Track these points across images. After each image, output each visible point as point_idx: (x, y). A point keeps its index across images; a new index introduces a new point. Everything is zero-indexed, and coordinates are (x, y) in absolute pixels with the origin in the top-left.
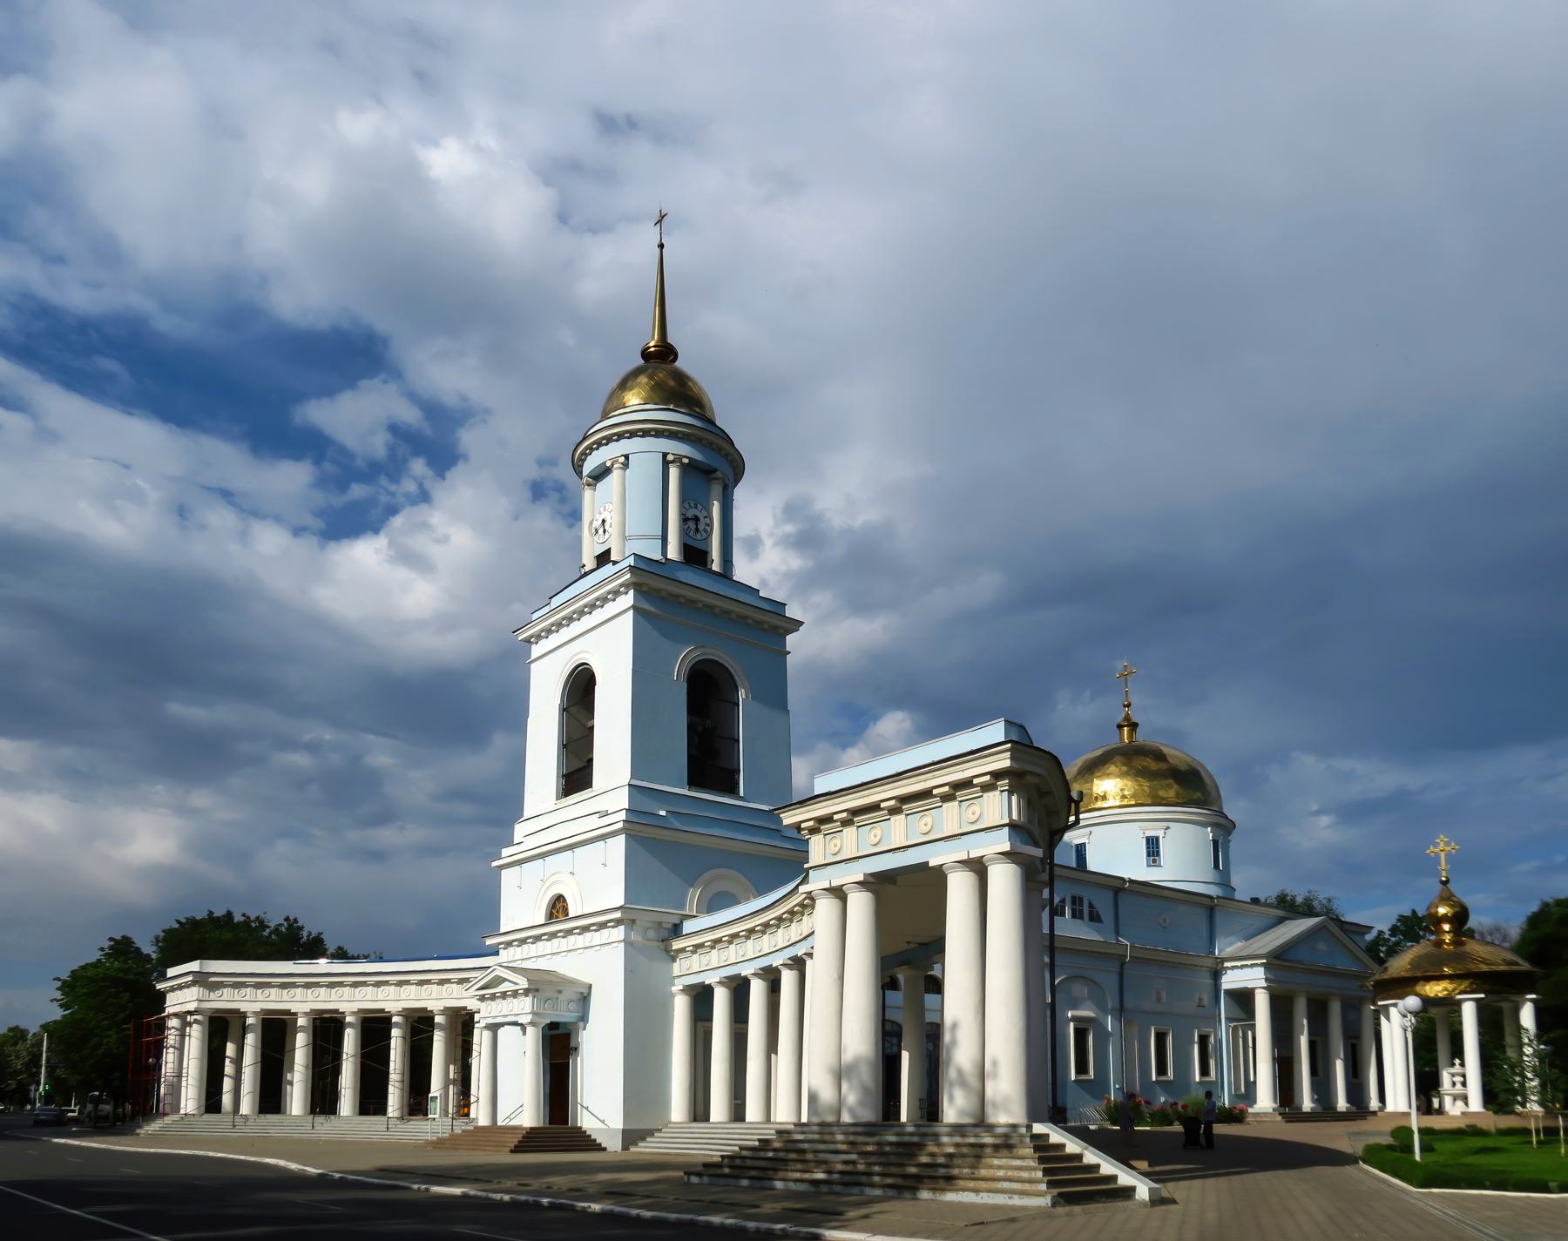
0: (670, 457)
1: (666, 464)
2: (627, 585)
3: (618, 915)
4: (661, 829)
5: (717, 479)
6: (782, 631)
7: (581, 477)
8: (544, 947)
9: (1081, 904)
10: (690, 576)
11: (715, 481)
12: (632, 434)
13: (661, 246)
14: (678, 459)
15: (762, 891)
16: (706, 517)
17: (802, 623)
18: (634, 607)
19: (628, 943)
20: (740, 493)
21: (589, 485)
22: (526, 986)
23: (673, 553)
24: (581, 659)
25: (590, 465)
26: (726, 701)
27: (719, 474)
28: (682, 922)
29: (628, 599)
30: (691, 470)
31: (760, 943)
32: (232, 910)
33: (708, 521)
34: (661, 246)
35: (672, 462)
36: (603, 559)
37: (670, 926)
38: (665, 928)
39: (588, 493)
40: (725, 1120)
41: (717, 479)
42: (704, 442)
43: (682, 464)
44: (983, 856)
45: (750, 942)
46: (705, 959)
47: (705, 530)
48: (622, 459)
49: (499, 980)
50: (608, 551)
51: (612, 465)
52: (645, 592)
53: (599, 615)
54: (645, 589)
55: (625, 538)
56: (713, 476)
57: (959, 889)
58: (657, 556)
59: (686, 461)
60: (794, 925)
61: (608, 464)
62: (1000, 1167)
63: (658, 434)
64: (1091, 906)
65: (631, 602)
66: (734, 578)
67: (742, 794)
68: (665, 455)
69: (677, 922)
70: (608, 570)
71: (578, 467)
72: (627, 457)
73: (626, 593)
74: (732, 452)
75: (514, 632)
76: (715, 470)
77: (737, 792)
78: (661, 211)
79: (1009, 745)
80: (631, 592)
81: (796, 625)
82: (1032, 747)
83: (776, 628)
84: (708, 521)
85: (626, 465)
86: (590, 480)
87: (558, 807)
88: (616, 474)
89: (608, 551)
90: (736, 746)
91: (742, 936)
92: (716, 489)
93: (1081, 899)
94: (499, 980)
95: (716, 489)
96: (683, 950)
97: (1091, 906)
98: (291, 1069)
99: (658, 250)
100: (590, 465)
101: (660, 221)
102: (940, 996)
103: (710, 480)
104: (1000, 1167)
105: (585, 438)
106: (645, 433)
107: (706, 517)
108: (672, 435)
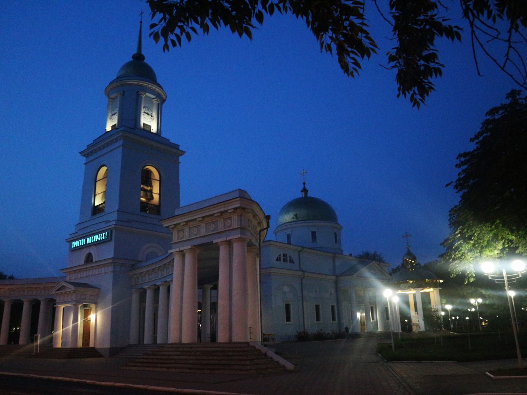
3: (110, 261)
8: (84, 274)
9: (287, 257)
13: (141, 22)
17: (185, 152)
19: (114, 272)
22: (74, 290)
29: (121, 142)
32: (271, 217)
34: (141, 22)
40: (151, 343)
44: (232, 239)
49: (63, 287)
53: (111, 148)
57: (223, 253)
62: (216, 360)
64: (290, 257)
66: (162, 136)
79: (239, 199)
81: (183, 153)
82: (252, 200)
87: (91, 219)
90: (101, 206)
93: (286, 255)
94: (63, 287)
97: (290, 257)
98: (406, 294)
99: (140, 24)
102: (216, 291)
104: (216, 360)
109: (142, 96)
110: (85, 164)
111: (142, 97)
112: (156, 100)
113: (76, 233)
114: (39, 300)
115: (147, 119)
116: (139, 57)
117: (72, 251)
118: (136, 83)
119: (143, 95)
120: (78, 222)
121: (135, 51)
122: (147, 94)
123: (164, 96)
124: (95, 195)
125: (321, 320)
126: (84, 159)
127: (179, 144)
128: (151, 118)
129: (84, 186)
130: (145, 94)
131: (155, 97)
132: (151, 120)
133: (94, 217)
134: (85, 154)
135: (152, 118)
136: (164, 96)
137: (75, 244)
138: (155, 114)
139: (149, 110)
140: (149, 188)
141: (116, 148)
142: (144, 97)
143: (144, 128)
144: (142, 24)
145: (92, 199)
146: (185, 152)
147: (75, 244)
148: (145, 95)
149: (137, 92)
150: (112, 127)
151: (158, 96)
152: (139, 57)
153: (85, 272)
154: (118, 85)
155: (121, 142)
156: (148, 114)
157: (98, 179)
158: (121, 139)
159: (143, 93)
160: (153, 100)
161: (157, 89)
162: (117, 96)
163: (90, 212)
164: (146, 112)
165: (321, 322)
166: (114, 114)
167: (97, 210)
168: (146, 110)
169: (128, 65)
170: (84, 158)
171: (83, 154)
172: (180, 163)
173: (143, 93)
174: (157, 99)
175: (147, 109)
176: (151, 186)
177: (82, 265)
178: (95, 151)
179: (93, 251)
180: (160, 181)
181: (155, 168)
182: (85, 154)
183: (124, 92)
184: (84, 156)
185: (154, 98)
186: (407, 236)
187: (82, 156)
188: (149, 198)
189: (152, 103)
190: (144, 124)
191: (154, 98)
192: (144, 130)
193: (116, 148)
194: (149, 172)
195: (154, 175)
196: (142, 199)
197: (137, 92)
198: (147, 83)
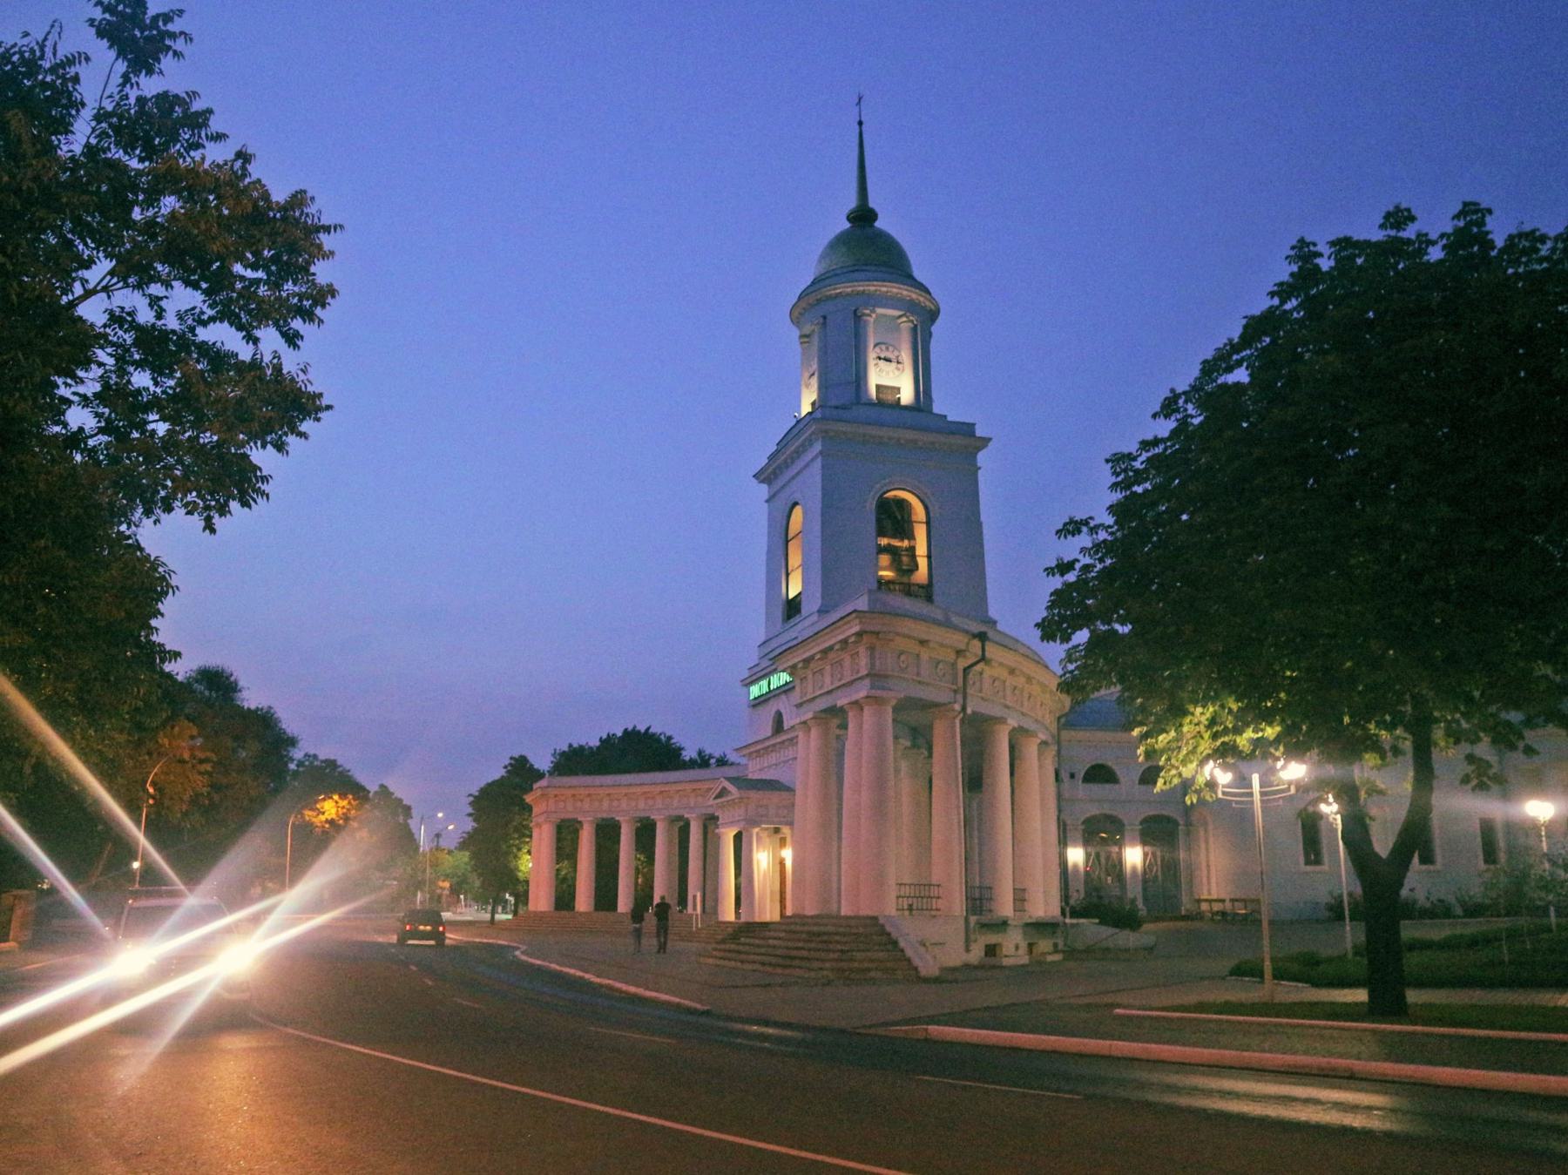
8: (773, 758)
13: (860, 123)
22: (738, 796)
34: (860, 123)
53: (800, 464)
81: (985, 441)
99: (857, 127)
109: (865, 318)
110: (767, 501)
111: (865, 321)
112: (904, 319)
113: (757, 665)
114: (687, 819)
115: (888, 373)
116: (863, 216)
117: (754, 706)
118: (849, 290)
119: (870, 315)
120: (763, 639)
121: (852, 203)
122: (880, 311)
123: (928, 303)
124: (787, 575)
125: (1439, 858)
126: (763, 490)
127: (971, 421)
128: (898, 369)
129: (769, 552)
130: (874, 312)
131: (901, 313)
132: (897, 373)
133: (792, 622)
134: (766, 476)
135: (900, 366)
136: (928, 303)
137: (755, 691)
138: (906, 357)
139: (891, 349)
140: (906, 543)
141: (807, 466)
142: (872, 320)
143: (881, 395)
144: (863, 126)
145: (781, 583)
146: (990, 439)
147: (755, 691)
148: (874, 315)
149: (855, 311)
150: (813, 404)
151: (911, 307)
152: (863, 216)
153: (773, 754)
154: (811, 301)
155: (818, 447)
156: (888, 360)
157: (791, 535)
158: (817, 440)
159: (868, 312)
160: (900, 321)
161: (905, 293)
162: (813, 331)
163: (779, 613)
164: (882, 356)
165: (1438, 866)
166: (813, 374)
167: (793, 608)
168: (882, 350)
169: (841, 240)
170: (764, 487)
171: (762, 477)
172: (980, 468)
173: (868, 312)
174: (907, 317)
175: (883, 347)
176: (911, 537)
177: (768, 738)
178: (787, 465)
179: (783, 705)
180: (928, 523)
181: (913, 494)
182: (766, 476)
183: (825, 318)
184: (762, 482)
185: (900, 317)
186: (185, 1113)
187: (760, 482)
188: (904, 567)
189: (898, 329)
190: (878, 387)
191: (900, 317)
192: (880, 403)
193: (807, 466)
194: (902, 504)
195: (916, 514)
196: (881, 573)
197: (855, 311)
198: (875, 283)
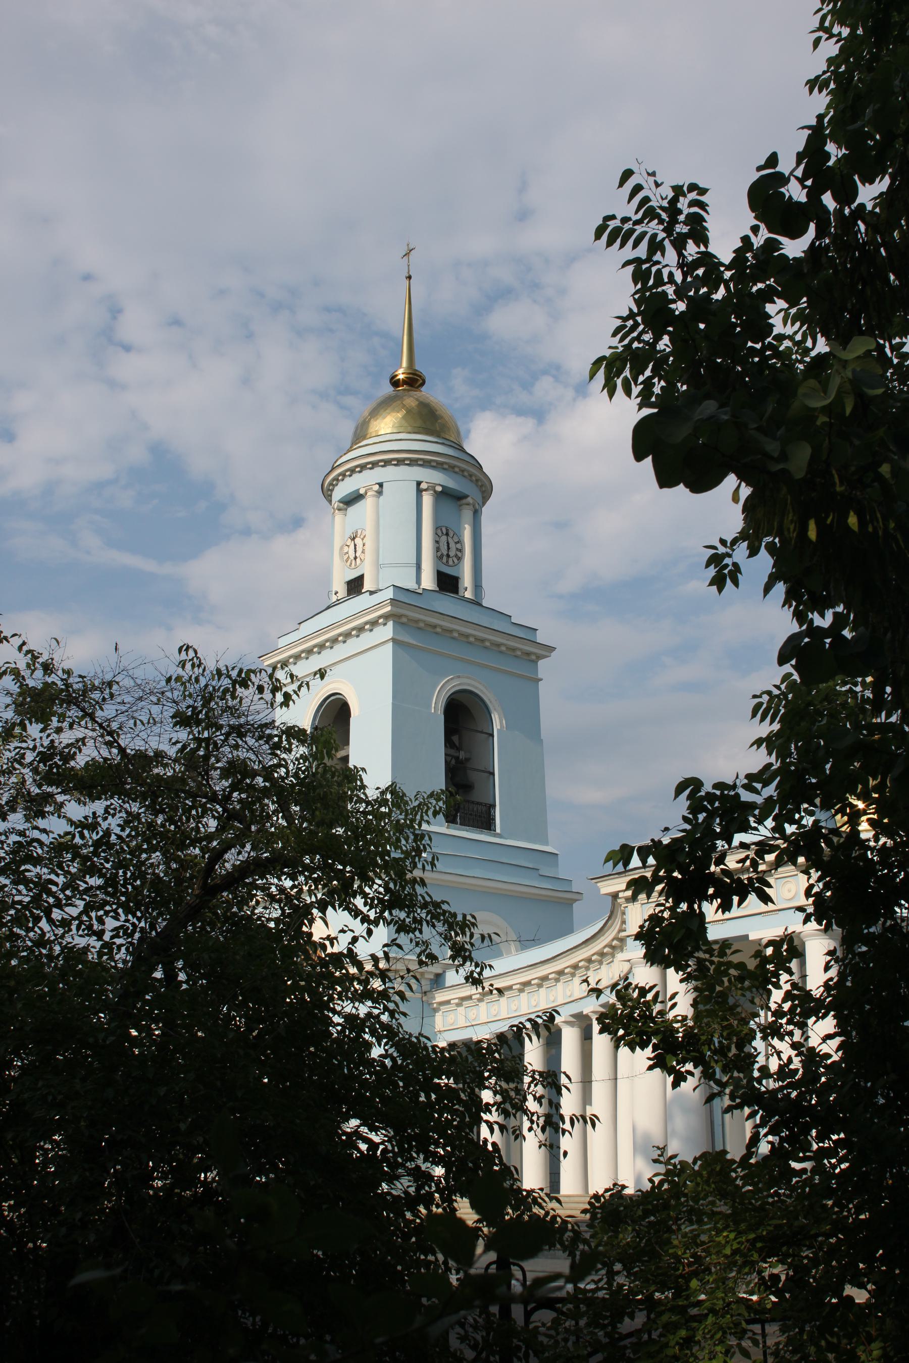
0: (424, 486)
1: (419, 491)
2: (386, 617)
4: (443, 875)
5: (468, 504)
6: (533, 657)
7: (330, 502)
10: (446, 604)
11: (467, 506)
12: (387, 463)
14: (432, 488)
15: (526, 942)
16: (456, 543)
18: (394, 640)
20: (487, 511)
21: (339, 510)
23: (428, 581)
24: (328, 691)
25: (342, 491)
26: (482, 732)
27: (469, 500)
28: (444, 972)
30: (445, 496)
31: (516, 1002)
33: (459, 546)
35: (426, 490)
36: (355, 586)
37: (432, 977)
38: (427, 979)
39: (339, 516)
41: (468, 504)
42: (457, 470)
43: (435, 491)
45: (542, 991)
46: (472, 1013)
47: (456, 556)
48: (377, 487)
50: (361, 578)
51: (366, 493)
52: (403, 624)
53: (354, 645)
54: (404, 620)
55: (378, 566)
56: (464, 501)
58: (411, 585)
59: (439, 489)
60: (604, 967)
61: (362, 491)
63: (413, 463)
65: (390, 635)
67: (498, 830)
68: (419, 483)
69: (439, 971)
70: (361, 602)
71: (327, 493)
72: (381, 485)
73: (385, 624)
74: (482, 477)
75: (260, 657)
76: (466, 497)
77: (493, 827)
78: (408, 245)
80: (390, 624)
83: (528, 654)
84: (459, 546)
85: (380, 493)
86: (341, 505)
88: (368, 503)
89: (361, 578)
91: (551, 979)
92: (467, 514)
95: (467, 514)
96: (448, 1002)
100: (342, 491)
101: (407, 254)
103: (460, 506)
105: (333, 469)
106: (400, 462)
107: (456, 543)
108: (426, 464)
146: (748, 557)
